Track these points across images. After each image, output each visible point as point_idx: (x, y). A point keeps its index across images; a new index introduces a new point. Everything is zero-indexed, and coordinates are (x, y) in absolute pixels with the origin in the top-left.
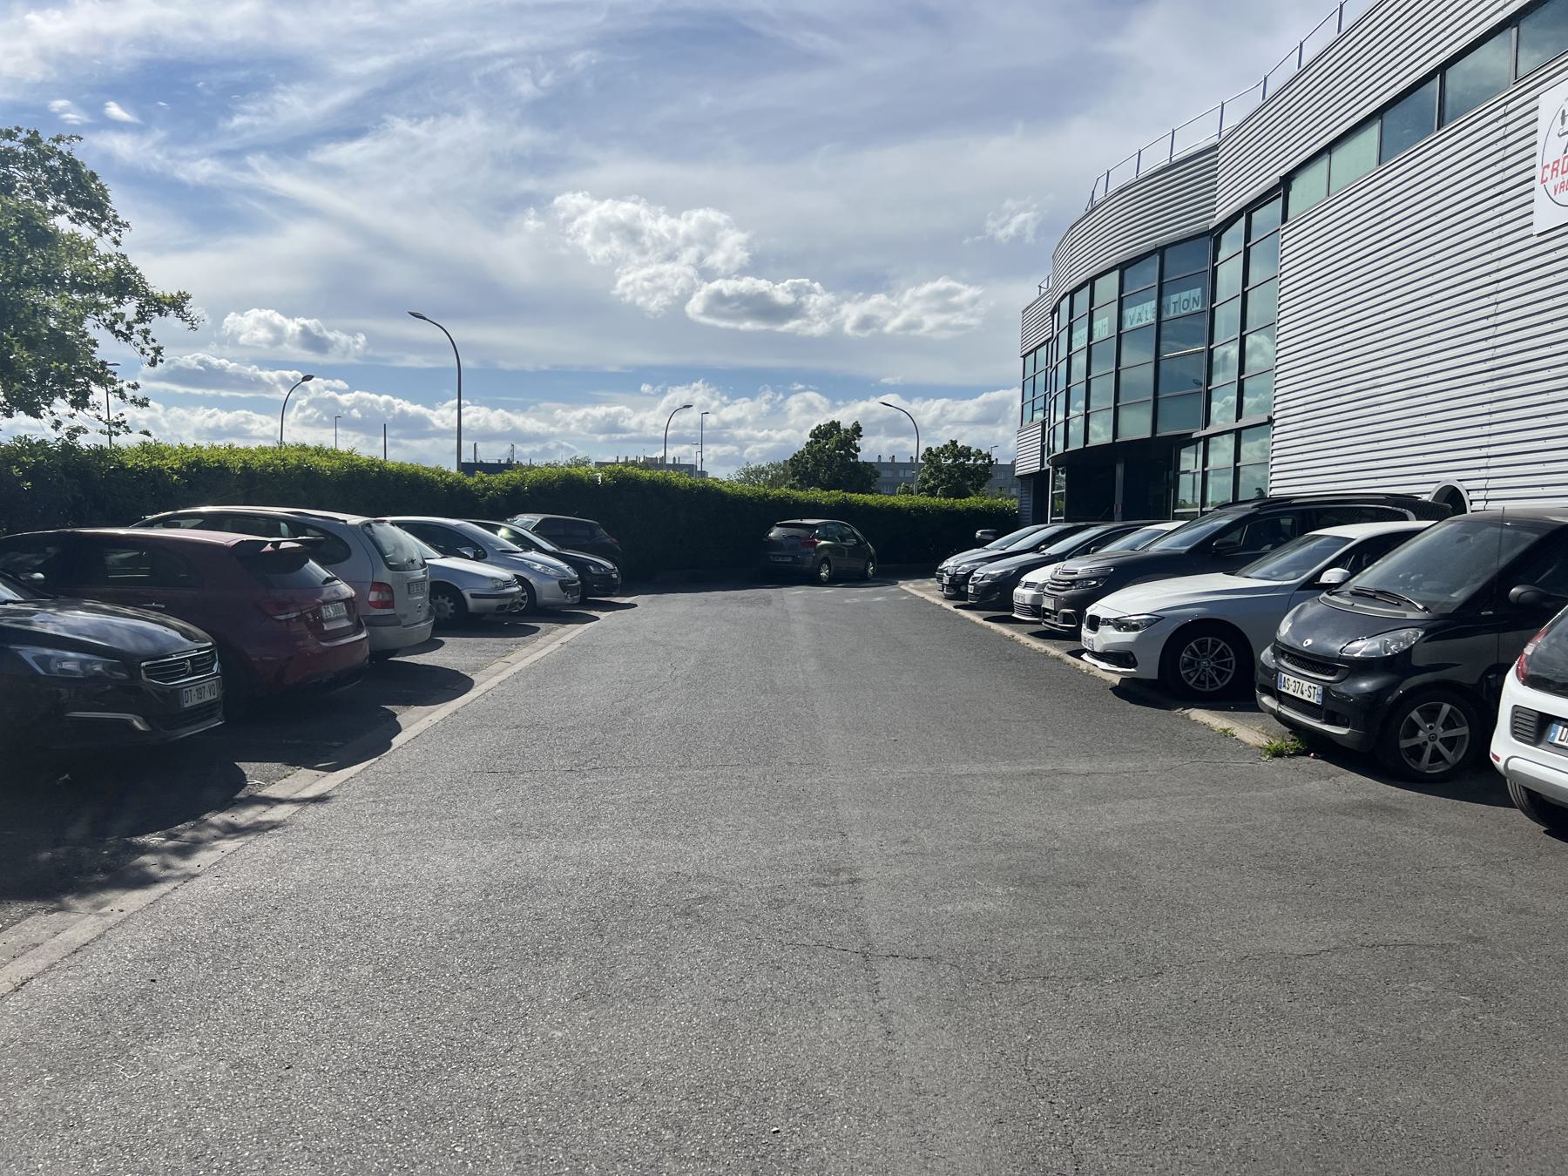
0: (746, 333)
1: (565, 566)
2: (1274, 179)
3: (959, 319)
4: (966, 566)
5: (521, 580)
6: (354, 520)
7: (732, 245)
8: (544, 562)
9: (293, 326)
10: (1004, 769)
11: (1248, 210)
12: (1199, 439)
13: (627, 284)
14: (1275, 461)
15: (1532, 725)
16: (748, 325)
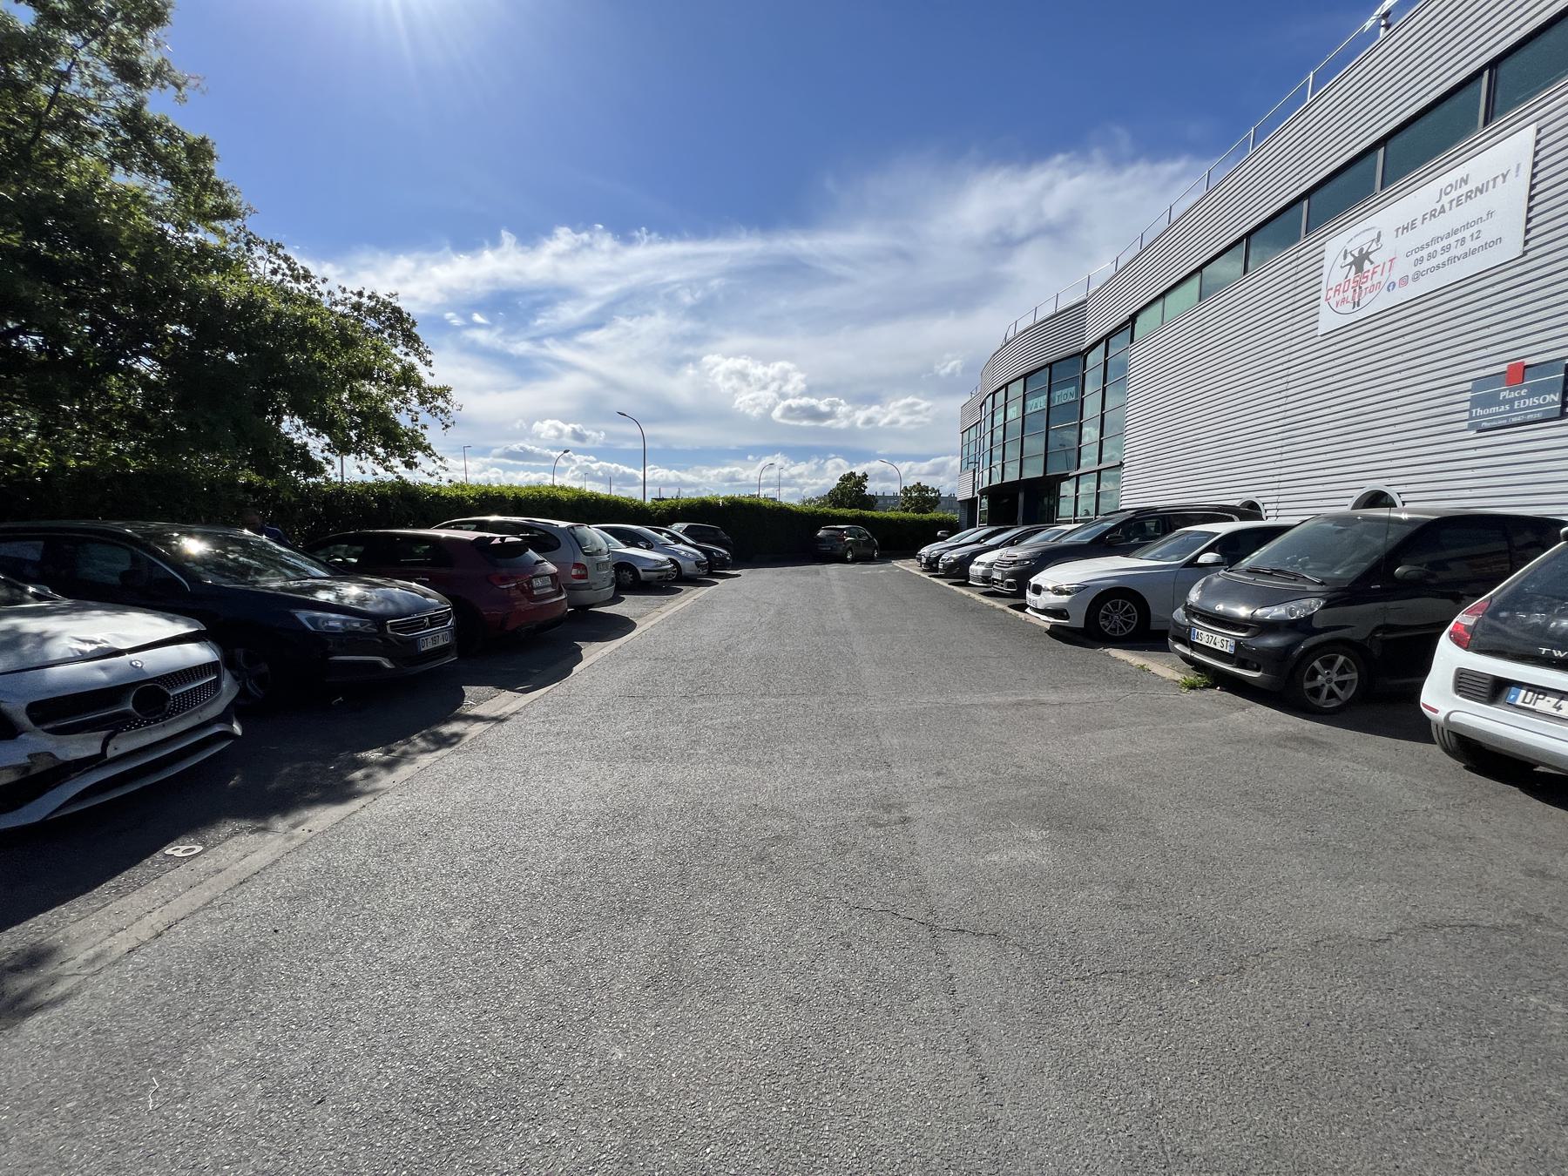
0: (803, 427)
1: (699, 553)
2: (1126, 317)
3: (919, 418)
4: (936, 552)
5: (672, 561)
6: (563, 524)
7: (797, 381)
8: (687, 551)
9: (568, 428)
10: (997, 699)
11: (1107, 338)
12: (1073, 476)
13: (741, 403)
14: (1124, 488)
15: (1486, 689)
16: (805, 423)
